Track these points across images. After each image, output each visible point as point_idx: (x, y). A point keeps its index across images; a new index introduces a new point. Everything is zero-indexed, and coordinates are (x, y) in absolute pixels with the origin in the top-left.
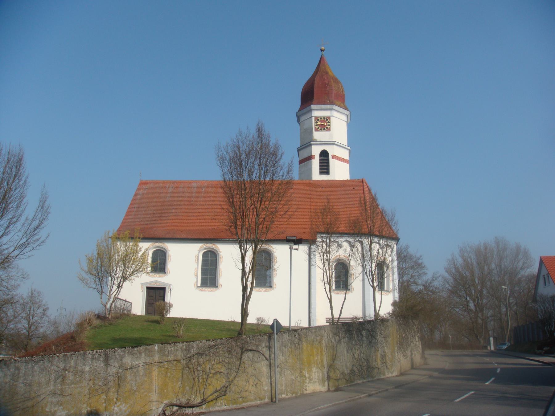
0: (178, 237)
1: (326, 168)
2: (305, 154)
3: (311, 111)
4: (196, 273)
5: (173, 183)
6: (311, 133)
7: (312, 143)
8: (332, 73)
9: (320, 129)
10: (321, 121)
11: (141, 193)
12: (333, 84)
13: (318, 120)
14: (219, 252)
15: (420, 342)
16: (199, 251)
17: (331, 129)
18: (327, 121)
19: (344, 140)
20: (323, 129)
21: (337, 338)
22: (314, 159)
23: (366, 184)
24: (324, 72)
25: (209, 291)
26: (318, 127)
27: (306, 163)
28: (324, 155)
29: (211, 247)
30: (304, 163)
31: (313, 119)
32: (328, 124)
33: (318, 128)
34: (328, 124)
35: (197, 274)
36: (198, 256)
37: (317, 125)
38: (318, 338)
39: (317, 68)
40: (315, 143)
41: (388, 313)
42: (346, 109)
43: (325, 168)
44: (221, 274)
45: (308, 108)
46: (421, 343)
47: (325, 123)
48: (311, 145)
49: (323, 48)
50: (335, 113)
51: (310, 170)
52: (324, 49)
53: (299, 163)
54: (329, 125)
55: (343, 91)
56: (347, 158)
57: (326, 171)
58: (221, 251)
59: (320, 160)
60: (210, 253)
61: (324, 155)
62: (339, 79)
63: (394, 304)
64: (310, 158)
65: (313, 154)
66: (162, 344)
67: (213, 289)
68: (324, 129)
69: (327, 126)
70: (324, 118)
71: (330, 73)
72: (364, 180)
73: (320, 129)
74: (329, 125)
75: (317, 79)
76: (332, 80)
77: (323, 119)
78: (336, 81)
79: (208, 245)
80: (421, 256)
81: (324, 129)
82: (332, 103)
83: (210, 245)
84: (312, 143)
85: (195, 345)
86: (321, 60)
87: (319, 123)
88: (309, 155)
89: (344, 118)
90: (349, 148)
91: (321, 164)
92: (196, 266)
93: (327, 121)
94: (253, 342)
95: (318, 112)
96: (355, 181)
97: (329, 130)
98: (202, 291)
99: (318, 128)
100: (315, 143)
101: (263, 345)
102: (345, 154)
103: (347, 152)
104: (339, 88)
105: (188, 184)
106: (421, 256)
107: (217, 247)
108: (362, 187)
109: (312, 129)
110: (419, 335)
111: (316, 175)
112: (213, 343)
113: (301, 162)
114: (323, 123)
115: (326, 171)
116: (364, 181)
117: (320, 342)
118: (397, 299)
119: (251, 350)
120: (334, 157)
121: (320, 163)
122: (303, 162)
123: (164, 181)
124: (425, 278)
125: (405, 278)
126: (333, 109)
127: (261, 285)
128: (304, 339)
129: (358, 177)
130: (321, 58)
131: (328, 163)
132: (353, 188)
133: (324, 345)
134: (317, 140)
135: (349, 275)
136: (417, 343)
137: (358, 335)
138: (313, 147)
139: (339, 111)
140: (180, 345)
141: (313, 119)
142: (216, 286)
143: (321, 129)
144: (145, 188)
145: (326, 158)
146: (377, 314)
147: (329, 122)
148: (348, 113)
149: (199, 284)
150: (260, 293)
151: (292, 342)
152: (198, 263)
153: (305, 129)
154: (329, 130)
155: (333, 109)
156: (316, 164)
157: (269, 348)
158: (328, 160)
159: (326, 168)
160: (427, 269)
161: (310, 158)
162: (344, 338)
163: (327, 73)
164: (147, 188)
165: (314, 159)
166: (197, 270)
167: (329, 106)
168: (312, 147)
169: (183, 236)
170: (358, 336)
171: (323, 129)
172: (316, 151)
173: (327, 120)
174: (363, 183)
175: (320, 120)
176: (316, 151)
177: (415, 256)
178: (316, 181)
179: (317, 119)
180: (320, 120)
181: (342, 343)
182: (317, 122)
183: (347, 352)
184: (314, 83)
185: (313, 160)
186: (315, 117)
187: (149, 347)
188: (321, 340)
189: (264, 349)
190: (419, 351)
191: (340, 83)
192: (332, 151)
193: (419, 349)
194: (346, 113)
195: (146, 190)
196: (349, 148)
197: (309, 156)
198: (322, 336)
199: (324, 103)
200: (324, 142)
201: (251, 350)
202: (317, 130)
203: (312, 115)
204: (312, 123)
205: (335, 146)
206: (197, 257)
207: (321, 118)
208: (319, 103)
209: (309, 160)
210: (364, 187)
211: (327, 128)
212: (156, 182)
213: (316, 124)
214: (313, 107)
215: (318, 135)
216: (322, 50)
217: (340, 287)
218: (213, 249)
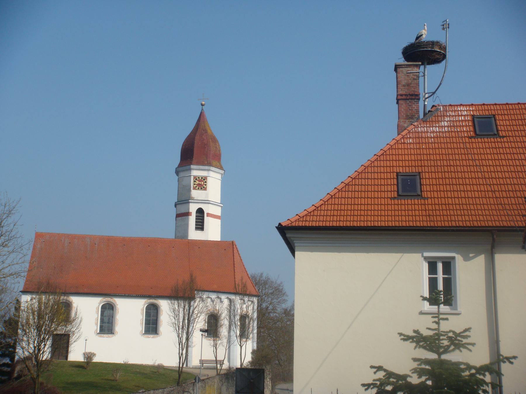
0: (82, 291)
1: (200, 224)
2: (182, 209)
3: (190, 170)
4: (96, 322)
5: (68, 236)
6: (190, 191)
7: (190, 201)
8: (211, 131)
9: (197, 188)
10: (200, 181)
11: (39, 246)
12: (211, 144)
13: (196, 179)
14: (116, 305)
15: (271, 382)
16: (100, 304)
17: (208, 188)
18: (204, 181)
19: (218, 199)
20: (200, 188)
21: (221, 383)
22: (191, 216)
23: (236, 246)
24: (204, 130)
25: (107, 337)
26: (195, 186)
27: (183, 217)
28: (200, 212)
29: (109, 301)
30: (181, 218)
31: (192, 177)
32: (205, 183)
33: (196, 187)
34: (205, 183)
35: (97, 323)
36: (98, 308)
37: (195, 184)
38: (213, 384)
39: (196, 123)
40: (193, 201)
41: (249, 362)
42: (221, 168)
43: (200, 226)
44: (117, 323)
45: (188, 167)
46: (271, 383)
47: (202, 183)
48: (189, 202)
49: (203, 103)
50: (211, 174)
51: (187, 226)
52: (205, 104)
53: (176, 216)
54: (206, 185)
55: (219, 151)
56: (219, 214)
57: (200, 227)
58: (117, 304)
59: (196, 216)
60: (108, 305)
61: (200, 212)
62: (218, 137)
63: (253, 352)
64: (187, 214)
65: (190, 211)
66: (154, 390)
67: (110, 335)
68: (201, 188)
69: (204, 186)
70: (202, 178)
71: (209, 131)
72: (234, 242)
73: (197, 188)
74: (206, 185)
75: (197, 138)
76: (210, 140)
77: (200, 178)
78: (215, 140)
79: (107, 299)
80: (281, 283)
81: (201, 188)
82: (210, 164)
83: (108, 299)
84: (190, 201)
85: (166, 390)
86: (202, 115)
87: (197, 182)
88: (187, 211)
89: (219, 176)
90: (222, 205)
91: (197, 218)
92: (97, 316)
93: (204, 181)
94: (187, 387)
95: (196, 172)
96: (227, 243)
97: (205, 189)
98: (101, 337)
99: (196, 187)
100: (193, 201)
101: (191, 389)
102: (217, 211)
103: (220, 208)
104: (216, 147)
105: (82, 238)
106: (281, 283)
107: (115, 301)
108: (232, 249)
109: (191, 187)
110: (270, 376)
111: (194, 235)
112: (172, 389)
113: (178, 216)
114: (200, 183)
115: (200, 227)
116: (234, 244)
117: (214, 386)
118: (255, 348)
119: (186, 392)
120: (208, 215)
121: (196, 219)
122: (180, 217)
123: (59, 234)
124: (284, 306)
125: (264, 305)
126: (210, 170)
127: (149, 332)
128: (207, 385)
129: (229, 239)
130: (201, 112)
131: (203, 219)
132: (225, 250)
133: (216, 387)
134: (194, 198)
135: (219, 325)
136: (268, 383)
137: (232, 380)
138: (191, 204)
139: (215, 171)
140: (160, 390)
141: (192, 177)
142: (112, 333)
143: (198, 188)
144: (41, 240)
145: (201, 216)
146: (242, 364)
147: (206, 182)
148: (222, 172)
149: (98, 331)
150: (148, 339)
151: (202, 387)
152: (98, 313)
153: (183, 185)
154: (205, 189)
155: (210, 170)
156: (192, 220)
157: (193, 390)
158: (203, 217)
159: (200, 224)
160: (287, 296)
161: (188, 214)
162: (225, 382)
163: (206, 131)
164: (43, 241)
165: (191, 216)
166: (97, 320)
167: (206, 167)
168: (189, 205)
169: (86, 290)
170: (232, 381)
171: (200, 188)
172: (193, 208)
173: (204, 180)
174: (233, 245)
175: (198, 179)
176: (193, 208)
177: (276, 281)
178: (194, 241)
179: (195, 178)
180: (198, 179)
181: (224, 386)
182: (195, 181)
183: (226, 391)
184: (194, 143)
185: (190, 217)
186: (193, 176)
187: (149, 392)
188: (214, 384)
189: (191, 391)
190: (269, 389)
191: (218, 141)
192: (207, 209)
193: (269, 387)
194: (220, 172)
195: (44, 243)
196: (222, 205)
197: (186, 213)
198: (215, 383)
199: (203, 164)
200: (200, 201)
201: (186, 392)
202: (194, 189)
203: (191, 174)
204: (190, 182)
205: (210, 205)
206: (97, 309)
207: (199, 178)
208: (198, 163)
209: (186, 216)
210: (234, 249)
211: (204, 187)
212: (52, 235)
213: (194, 183)
214: (192, 167)
215: (196, 194)
216: (202, 105)
217: (211, 335)
218: (109, 301)
